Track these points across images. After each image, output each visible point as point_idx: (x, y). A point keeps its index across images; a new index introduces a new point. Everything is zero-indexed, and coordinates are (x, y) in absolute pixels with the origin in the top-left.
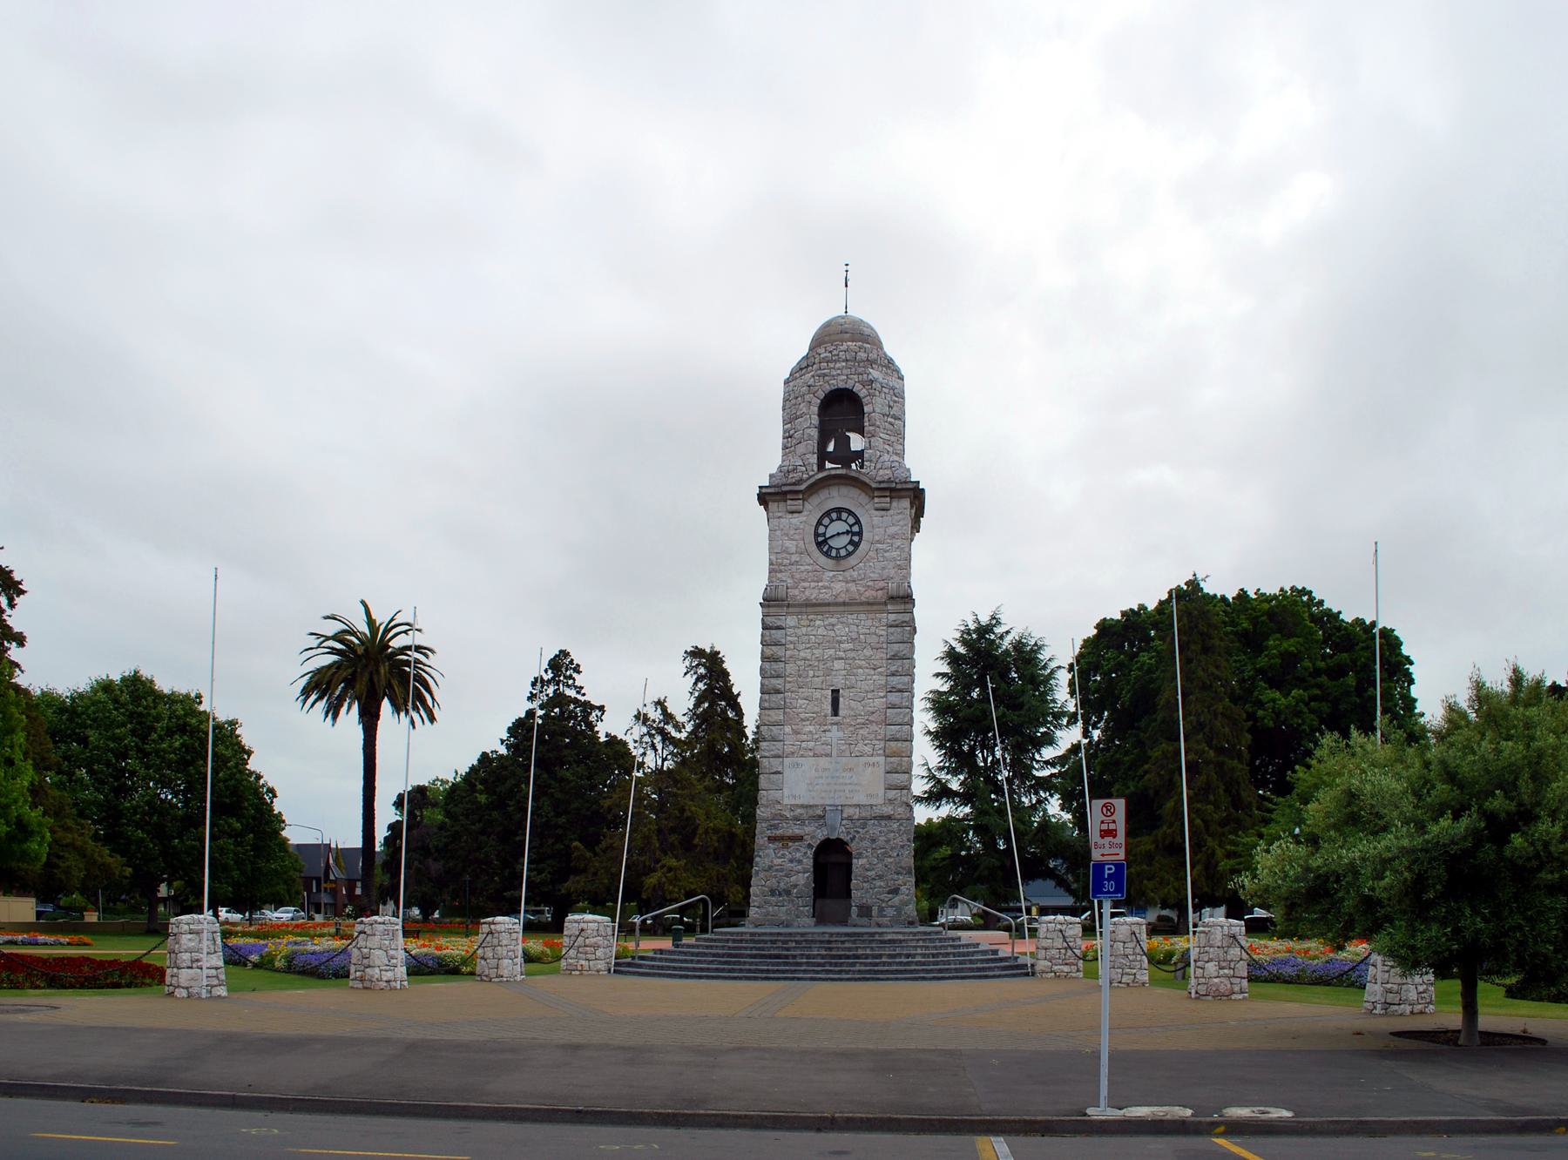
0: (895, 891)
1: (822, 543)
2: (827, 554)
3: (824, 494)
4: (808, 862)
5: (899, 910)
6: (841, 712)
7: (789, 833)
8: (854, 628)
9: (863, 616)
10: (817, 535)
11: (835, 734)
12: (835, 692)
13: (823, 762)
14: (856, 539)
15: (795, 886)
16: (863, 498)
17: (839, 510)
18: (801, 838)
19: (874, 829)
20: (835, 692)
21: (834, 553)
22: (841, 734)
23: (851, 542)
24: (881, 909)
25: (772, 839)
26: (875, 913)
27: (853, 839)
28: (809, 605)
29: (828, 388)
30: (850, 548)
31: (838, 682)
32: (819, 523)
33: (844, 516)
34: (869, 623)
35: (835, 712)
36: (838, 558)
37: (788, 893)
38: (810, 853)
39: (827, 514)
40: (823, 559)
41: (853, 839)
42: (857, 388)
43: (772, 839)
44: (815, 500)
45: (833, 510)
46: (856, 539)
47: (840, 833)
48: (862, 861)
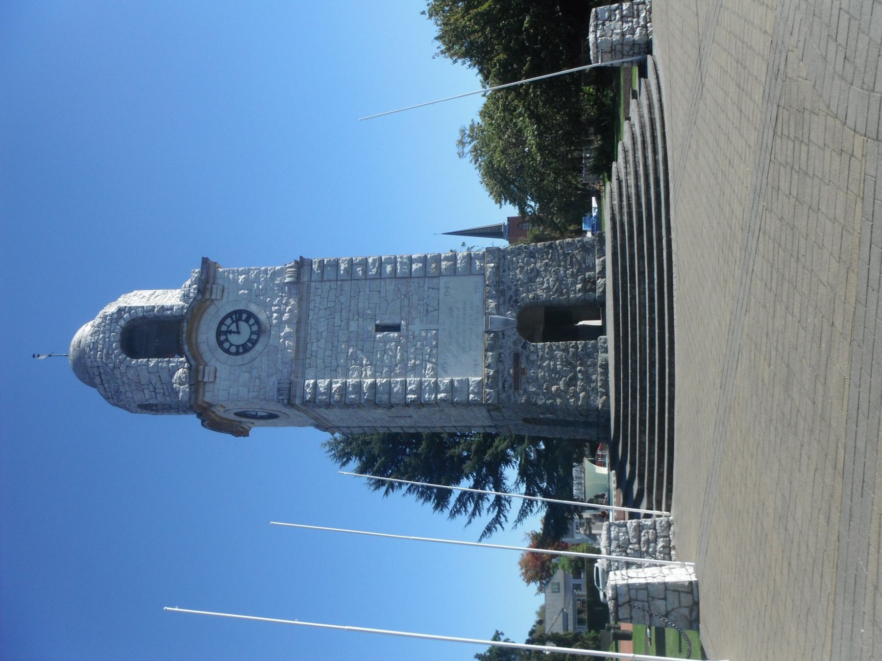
3: (203, 348)
8: (322, 313)
9: (312, 305)
10: (237, 353)
12: (380, 328)
14: (244, 316)
16: (212, 310)
18: (517, 357)
20: (396, 328)
21: (254, 337)
22: (417, 321)
23: (247, 321)
30: (252, 321)
31: (371, 328)
32: (227, 351)
34: (318, 299)
40: (259, 347)
44: (207, 357)
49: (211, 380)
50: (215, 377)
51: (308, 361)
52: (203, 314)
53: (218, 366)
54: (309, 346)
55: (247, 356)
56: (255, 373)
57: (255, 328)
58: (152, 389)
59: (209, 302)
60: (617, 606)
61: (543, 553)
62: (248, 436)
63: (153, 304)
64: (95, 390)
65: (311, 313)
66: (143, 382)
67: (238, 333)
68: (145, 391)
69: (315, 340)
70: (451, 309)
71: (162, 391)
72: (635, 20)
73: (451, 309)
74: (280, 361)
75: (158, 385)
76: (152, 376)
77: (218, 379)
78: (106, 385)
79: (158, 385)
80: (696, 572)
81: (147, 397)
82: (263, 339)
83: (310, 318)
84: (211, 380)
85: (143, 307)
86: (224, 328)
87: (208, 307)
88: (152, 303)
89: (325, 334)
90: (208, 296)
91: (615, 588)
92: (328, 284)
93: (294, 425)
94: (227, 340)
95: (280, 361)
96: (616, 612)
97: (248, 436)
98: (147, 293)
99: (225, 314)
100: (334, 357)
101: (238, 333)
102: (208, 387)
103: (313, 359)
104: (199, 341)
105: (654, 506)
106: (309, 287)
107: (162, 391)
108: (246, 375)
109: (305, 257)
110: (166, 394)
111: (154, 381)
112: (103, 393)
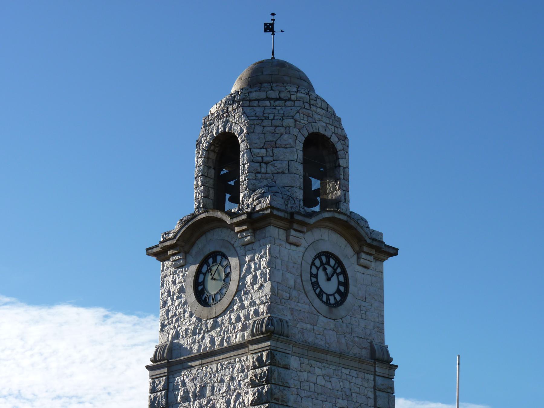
3: (200, 244)
8: (347, 385)
9: (354, 373)
17: (329, 255)
49: (292, 239)
50: (291, 244)
51: (306, 361)
52: (346, 239)
53: (301, 249)
54: (318, 364)
55: (309, 287)
56: (294, 293)
57: (332, 301)
58: (267, 159)
59: (357, 249)
62: (397, 255)
65: (347, 371)
66: (276, 151)
68: (263, 151)
69: (324, 372)
71: (263, 170)
74: (305, 326)
75: (270, 168)
76: (285, 164)
77: (288, 246)
82: (324, 308)
83: (343, 370)
84: (292, 239)
85: (347, 167)
86: (332, 262)
89: (328, 385)
90: (365, 249)
92: (371, 395)
93: (383, 308)
95: (305, 326)
97: (397, 255)
99: (346, 267)
100: (309, 394)
102: (282, 234)
103: (308, 368)
104: (323, 230)
106: (368, 372)
107: (263, 170)
108: (292, 283)
109: (397, 372)
110: (259, 176)
111: (278, 164)
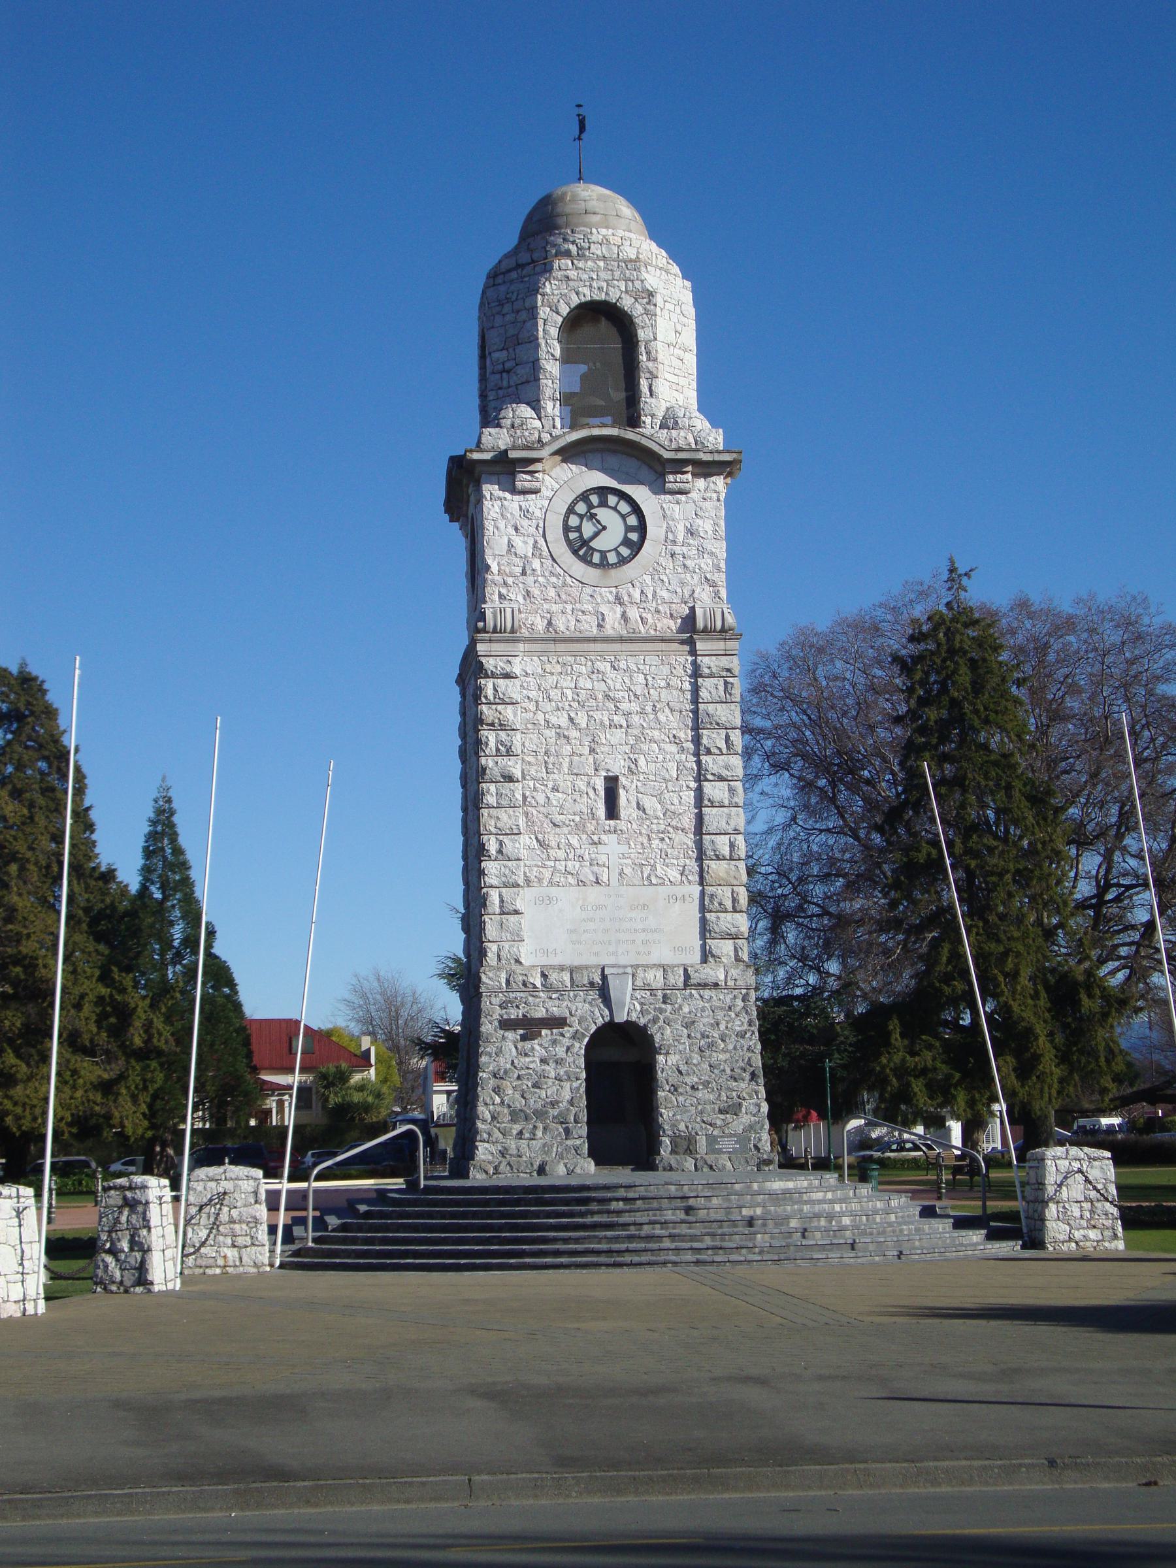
0: (733, 1109)
1: (581, 548)
2: (586, 560)
4: (577, 1063)
5: (742, 1139)
6: (600, 784)
7: (540, 1013)
11: (612, 848)
13: (594, 894)
15: (553, 1104)
18: (558, 1023)
19: (690, 1004)
21: (596, 558)
22: (624, 848)
24: (712, 1140)
25: (507, 1024)
26: (702, 1144)
27: (655, 1020)
28: (553, 639)
29: (575, 301)
30: (625, 552)
31: (617, 766)
33: (612, 500)
35: (612, 811)
36: (604, 565)
37: (540, 1114)
38: (580, 1048)
39: (642, 528)
40: (578, 568)
41: (655, 1020)
42: (627, 303)
43: (507, 1024)
45: (643, 537)
46: (594, 499)
47: (628, 1009)
48: (673, 1059)
52: (638, 459)
57: (612, 558)
58: (508, 365)
59: (660, 469)
60: (122, 1188)
61: (964, 946)
63: (660, 358)
64: (513, 240)
66: (518, 349)
67: (604, 528)
68: (505, 353)
70: (644, 906)
72: (1084, 1223)
73: (644, 906)
75: (514, 379)
78: (514, 275)
79: (514, 379)
80: (168, 1293)
81: (495, 355)
87: (651, 467)
88: (661, 350)
91: (144, 1187)
94: (603, 554)
96: (115, 1188)
98: (689, 337)
101: (604, 528)
105: (56, 1160)
107: (505, 384)
110: (501, 392)
112: (503, 267)
